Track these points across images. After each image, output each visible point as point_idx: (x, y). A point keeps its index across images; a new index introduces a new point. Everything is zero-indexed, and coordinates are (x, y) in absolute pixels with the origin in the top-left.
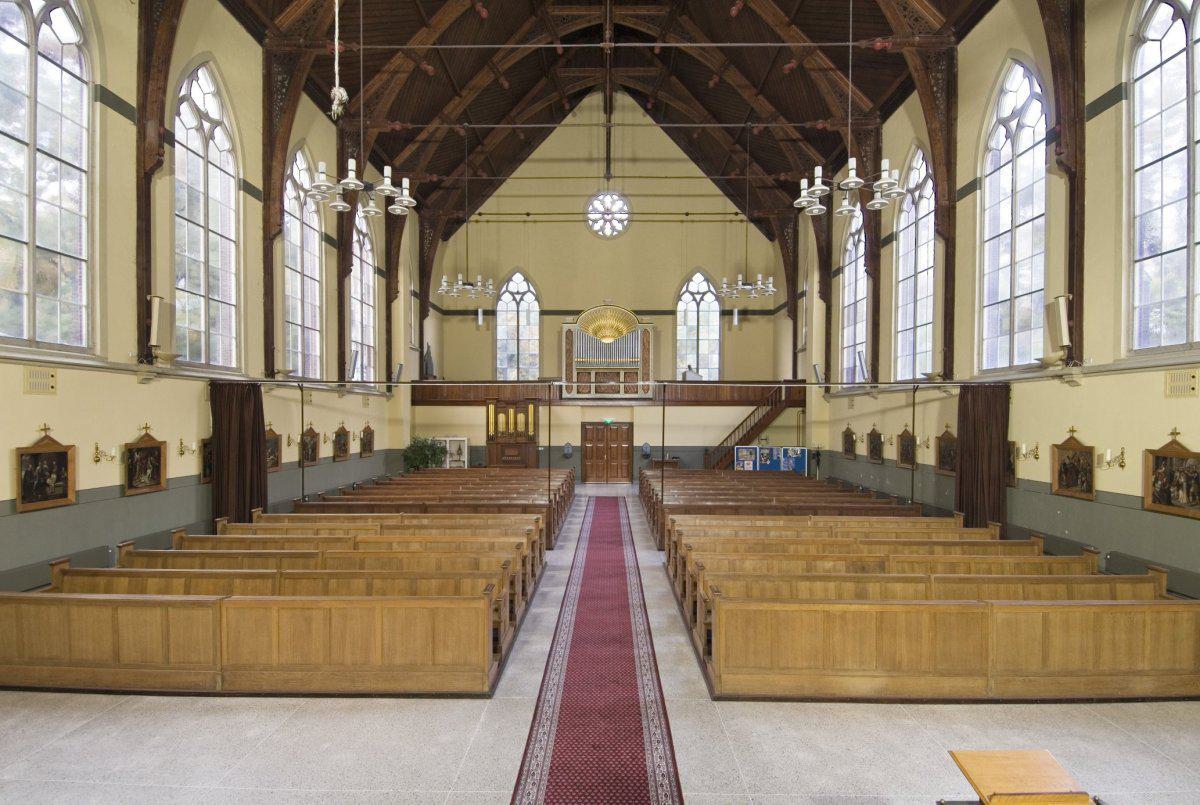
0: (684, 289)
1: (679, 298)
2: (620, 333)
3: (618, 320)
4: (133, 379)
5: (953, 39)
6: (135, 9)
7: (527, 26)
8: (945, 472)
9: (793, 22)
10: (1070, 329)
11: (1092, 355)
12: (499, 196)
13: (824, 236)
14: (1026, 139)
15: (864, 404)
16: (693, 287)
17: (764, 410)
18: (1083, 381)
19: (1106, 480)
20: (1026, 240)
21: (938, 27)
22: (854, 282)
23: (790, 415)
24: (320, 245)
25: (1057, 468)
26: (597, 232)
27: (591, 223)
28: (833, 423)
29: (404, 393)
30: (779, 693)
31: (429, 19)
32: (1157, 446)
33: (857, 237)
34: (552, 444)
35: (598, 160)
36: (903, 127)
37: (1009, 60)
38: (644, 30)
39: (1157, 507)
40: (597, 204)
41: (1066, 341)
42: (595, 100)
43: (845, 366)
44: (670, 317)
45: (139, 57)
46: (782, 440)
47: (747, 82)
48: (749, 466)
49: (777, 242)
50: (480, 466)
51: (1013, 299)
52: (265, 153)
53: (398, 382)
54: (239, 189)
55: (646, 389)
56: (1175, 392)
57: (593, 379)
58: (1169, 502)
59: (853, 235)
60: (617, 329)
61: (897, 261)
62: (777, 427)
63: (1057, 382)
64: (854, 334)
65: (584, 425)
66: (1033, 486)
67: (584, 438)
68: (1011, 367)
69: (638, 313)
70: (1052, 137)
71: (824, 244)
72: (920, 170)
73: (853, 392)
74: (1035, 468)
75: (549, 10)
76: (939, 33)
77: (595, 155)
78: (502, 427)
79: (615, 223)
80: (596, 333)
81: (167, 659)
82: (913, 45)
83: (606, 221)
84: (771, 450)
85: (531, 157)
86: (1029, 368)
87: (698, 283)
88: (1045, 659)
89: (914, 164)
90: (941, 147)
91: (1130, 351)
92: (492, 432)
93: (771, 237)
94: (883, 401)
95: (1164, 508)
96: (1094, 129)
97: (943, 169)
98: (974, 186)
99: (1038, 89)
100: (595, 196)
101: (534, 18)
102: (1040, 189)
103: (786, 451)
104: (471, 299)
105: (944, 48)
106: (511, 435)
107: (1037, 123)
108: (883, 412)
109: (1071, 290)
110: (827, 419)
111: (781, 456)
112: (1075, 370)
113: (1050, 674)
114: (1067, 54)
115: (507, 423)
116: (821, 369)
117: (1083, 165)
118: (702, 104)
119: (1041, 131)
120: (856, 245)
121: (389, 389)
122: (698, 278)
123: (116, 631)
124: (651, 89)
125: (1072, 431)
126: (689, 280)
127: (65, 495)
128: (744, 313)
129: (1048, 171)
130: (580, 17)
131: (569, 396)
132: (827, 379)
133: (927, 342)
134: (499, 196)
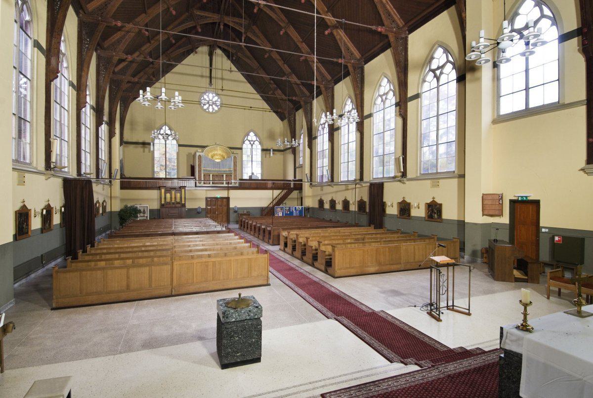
0: (246, 139)
1: (244, 142)
2: (224, 158)
3: (223, 151)
4: (43, 177)
5: (363, 63)
6: (46, 3)
7: (184, 17)
8: (361, 213)
9: (304, 42)
10: (403, 166)
11: (410, 175)
12: (155, 88)
13: (309, 123)
14: (388, 103)
15: (328, 189)
16: (249, 138)
17: (285, 191)
18: (407, 182)
19: (414, 213)
20: (388, 136)
21: (358, 58)
22: (322, 142)
23: (295, 194)
24: (90, 111)
25: (399, 209)
26: (205, 110)
27: (202, 105)
28: (313, 196)
29: (117, 183)
30: (352, 274)
31: (148, 9)
32: (429, 202)
33: (323, 126)
34: (112, 210)
35: (206, 77)
36: (343, 89)
37: (383, 76)
38: (238, 29)
39: (429, 219)
40: (205, 97)
41: (402, 171)
42: (204, 49)
43: (318, 174)
44: (240, 150)
45: (47, 26)
46: (292, 203)
47: (280, 58)
48: (281, 214)
49: (286, 121)
50: (154, 218)
51: (384, 155)
52: (78, 68)
53: (115, 179)
54: (70, 86)
55: (235, 183)
56: (433, 186)
57: (211, 179)
58: (432, 218)
59: (322, 125)
60: (222, 156)
61: (341, 137)
62: (291, 198)
63: (399, 183)
64: (323, 164)
65: (206, 198)
66: (392, 216)
67: (207, 205)
68: (383, 177)
69: (231, 148)
70: (397, 104)
71: (309, 127)
72: (349, 106)
73: (321, 185)
74: (392, 210)
75: (195, 12)
76: (359, 60)
77: (204, 74)
78: (168, 200)
79: (207, 105)
80: (212, 157)
81: (150, 285)
82: (351, 63)
83: (208, 103)
84: (290, 208)
85: (172, 71)
86: (389, 178)
87: (252, 136)
88: (414, 260)
89: (347, 103)
90: (359, 100)
91: (420, 174)
92: (163, 203)
93: (282, 119)
94: (335, 188)
95: (431, 220)
96: (411, 105)
97: (360, 108)
98: (370, 116)
99: (392, 88)
100: (205, 93)
101: (187, 14)
102: (393, 120)
103: (295, 208)
104: (139, 137)
105: (360, 66)
106: (173, 203)
107: (392, 99)
108: (337, 192)
109: (403, 154)
110: (311, 195)
111: (294, 210)
112: (405, 179)
113: (416, 262)
114: (403, 81)
115: (181, 198)
116: (309, 175)
117: (407, 116)
118: (257, 62)
119: (394, 102)
120: (323, 129)
121: (110, 182)
122: (252, 134)
123: (128, 277)
124: (235, 51)
125: (404, 198)
126: (248, 135)
127: (27, 233)
128: (274, 150)
129: (396, 115)
130: (209, 17)
131: (200, 185)
132: (311, 180)
133: (353, 167)
134: (155, 88)
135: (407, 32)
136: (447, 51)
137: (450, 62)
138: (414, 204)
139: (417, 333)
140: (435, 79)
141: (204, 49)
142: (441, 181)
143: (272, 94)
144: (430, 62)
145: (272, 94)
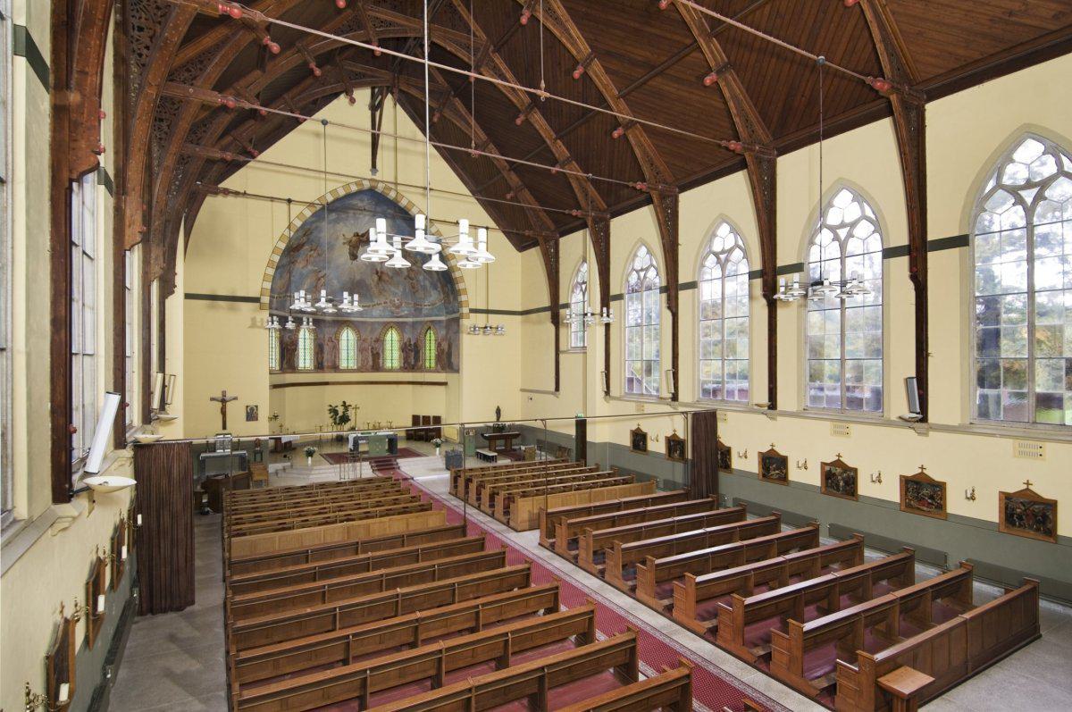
19: (794, 474)
33: (642, 274)
42: (363, 95)
112: (676, 403)
119: (744, 268)
135: (925, 97)
136: (735, 230)
137: (740, 248)
138: (651, 434)
139: (688, 652)
140: (836, 243)
141: (363, 95)
142: (728, 413)
143: (512, 199)
144: (711, 241)
145: (512, 199)
